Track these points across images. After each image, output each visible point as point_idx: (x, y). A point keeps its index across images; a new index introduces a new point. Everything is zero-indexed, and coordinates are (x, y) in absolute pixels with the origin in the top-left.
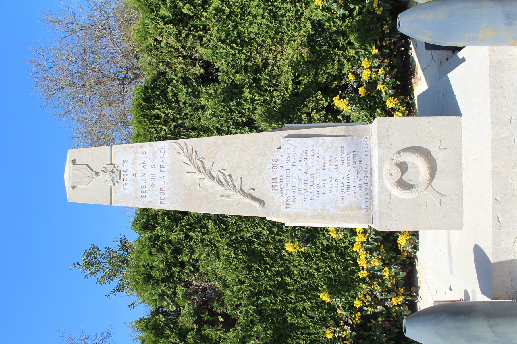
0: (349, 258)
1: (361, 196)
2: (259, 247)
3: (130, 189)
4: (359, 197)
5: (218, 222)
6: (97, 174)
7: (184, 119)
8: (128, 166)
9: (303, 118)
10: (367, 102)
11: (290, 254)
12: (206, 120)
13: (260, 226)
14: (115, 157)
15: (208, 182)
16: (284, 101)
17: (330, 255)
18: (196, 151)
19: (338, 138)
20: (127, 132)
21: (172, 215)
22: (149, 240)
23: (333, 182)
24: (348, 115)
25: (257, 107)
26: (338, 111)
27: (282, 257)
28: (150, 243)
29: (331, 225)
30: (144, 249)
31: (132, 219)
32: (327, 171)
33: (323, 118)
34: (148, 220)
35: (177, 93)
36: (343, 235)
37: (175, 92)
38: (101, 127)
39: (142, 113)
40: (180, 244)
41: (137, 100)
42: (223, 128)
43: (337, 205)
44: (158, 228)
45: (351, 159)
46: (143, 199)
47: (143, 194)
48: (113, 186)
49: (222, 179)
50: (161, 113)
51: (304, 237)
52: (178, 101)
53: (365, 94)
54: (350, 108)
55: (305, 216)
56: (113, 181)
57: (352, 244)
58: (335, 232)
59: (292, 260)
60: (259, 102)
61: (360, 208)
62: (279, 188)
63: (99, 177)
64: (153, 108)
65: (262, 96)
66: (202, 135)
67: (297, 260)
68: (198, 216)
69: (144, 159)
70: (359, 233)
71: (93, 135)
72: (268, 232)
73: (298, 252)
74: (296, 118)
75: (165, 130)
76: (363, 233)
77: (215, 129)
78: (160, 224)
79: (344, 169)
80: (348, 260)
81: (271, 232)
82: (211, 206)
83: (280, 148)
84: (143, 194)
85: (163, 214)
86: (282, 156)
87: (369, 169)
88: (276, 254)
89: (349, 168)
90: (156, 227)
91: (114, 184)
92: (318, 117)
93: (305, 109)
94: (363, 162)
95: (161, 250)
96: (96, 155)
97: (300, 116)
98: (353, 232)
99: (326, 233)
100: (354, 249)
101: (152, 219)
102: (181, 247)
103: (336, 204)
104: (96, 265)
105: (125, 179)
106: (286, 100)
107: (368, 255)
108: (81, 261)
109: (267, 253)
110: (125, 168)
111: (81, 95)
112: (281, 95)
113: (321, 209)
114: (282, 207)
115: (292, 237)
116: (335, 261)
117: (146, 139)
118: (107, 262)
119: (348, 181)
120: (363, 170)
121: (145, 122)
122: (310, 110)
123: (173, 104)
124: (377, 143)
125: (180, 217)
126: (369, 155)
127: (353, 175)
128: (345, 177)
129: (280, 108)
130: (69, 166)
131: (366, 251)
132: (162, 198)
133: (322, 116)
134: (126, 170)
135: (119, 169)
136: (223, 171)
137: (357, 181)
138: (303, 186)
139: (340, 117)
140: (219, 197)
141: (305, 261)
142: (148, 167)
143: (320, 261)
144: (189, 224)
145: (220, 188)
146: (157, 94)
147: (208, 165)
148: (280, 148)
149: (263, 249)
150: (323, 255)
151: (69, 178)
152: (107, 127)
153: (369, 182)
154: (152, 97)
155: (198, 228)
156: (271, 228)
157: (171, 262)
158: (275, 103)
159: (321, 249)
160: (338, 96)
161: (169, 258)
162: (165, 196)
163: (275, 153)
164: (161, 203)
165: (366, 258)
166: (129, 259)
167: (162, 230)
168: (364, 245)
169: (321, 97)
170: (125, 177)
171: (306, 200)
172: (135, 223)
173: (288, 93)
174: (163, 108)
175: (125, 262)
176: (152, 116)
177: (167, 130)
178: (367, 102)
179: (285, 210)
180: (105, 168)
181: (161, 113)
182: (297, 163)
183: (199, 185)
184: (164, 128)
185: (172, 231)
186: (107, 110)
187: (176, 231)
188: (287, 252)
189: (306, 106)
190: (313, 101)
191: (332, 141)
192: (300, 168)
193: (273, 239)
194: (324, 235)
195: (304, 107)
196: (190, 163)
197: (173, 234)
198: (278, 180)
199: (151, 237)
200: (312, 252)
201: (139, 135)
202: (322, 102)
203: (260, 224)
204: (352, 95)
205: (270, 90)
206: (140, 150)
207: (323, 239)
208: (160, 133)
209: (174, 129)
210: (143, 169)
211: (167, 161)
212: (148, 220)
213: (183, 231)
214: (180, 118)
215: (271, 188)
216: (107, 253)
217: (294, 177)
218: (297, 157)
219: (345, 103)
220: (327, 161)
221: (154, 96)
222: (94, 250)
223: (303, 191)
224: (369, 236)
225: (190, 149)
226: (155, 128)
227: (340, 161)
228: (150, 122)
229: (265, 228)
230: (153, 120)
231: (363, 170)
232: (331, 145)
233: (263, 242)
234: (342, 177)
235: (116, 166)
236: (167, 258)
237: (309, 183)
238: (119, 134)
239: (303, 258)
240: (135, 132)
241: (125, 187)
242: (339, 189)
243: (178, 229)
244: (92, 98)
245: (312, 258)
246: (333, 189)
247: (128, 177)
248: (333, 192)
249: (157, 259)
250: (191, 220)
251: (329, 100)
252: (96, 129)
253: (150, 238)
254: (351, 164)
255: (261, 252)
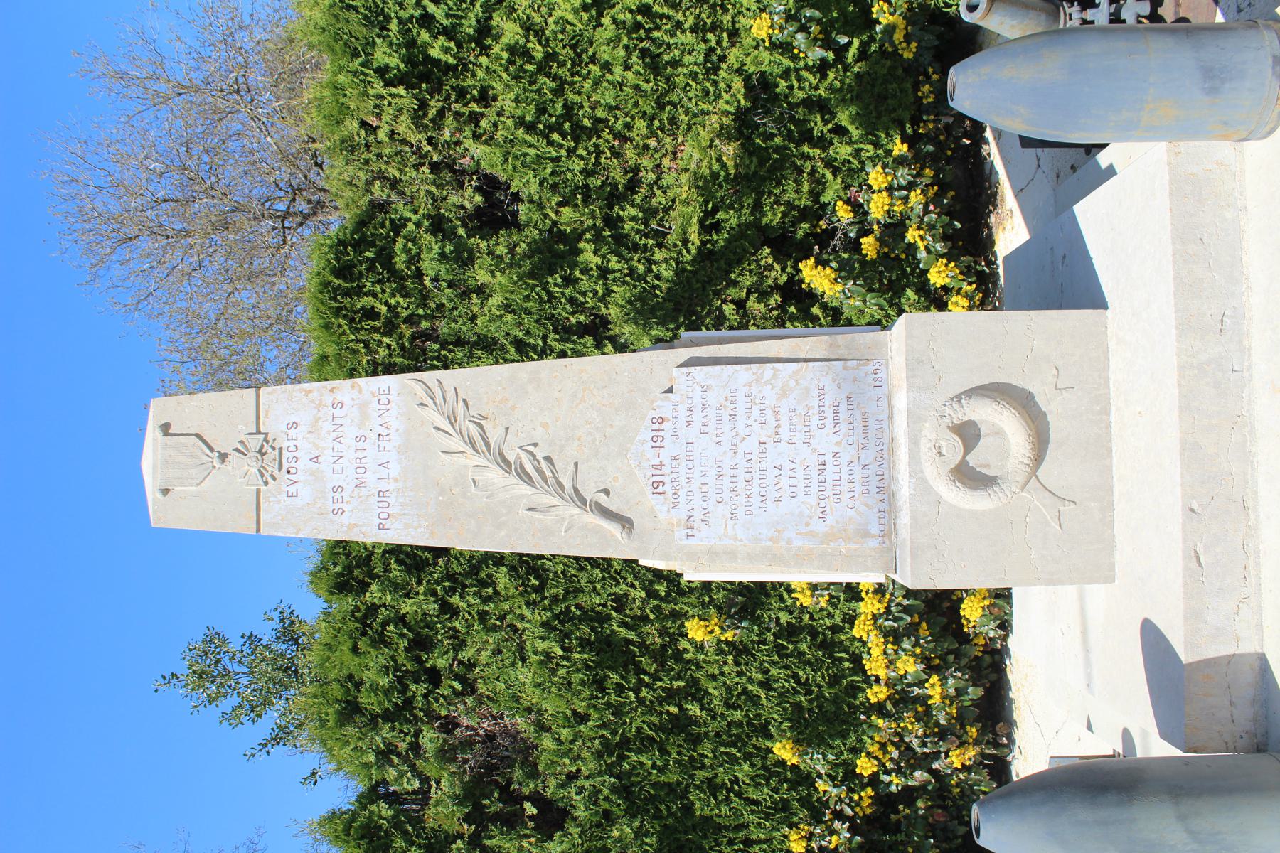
0: (843, 655)
1: (867, 506)
2: (623, 632)
3: (305, 493)
4: (863, 508)
5: (522, 571)
6: (223, 457)
7: (435, 317)
8: (300, 437)
9: (727, 313)
10: (881, 273)
11: (700, 647)
12: (489, 321)
13: (625, 579)
14: (266, 417)
15: (495, 475)
16: (679, 272)
17: (796, 648)
18: (465, 401)
19: (811, 364)
20: (294, 346)
21: (407, 554)
22: (353, 616)
23: (800, 473)
24: (835, 304)
25: (614, 288)
26: (811, 297)
27: (678, 655)
28: (353, 625)
29: (798, 578)
30: (341, 638)
31: (311, 566)
32: (783, 445)
33: (775, 313)
34: (349, 567)
35: (418, 254)
36: (827, 598)
37: (414, 252)
38: (230, 336)
39: (333, 304)
40: (427, 626)
41: (319, 274)
42: (532, 341)
43: (809, 529)
44: (374, 587)
45: (843, 415)
46: (336, 518)
47: (337, 506)
48: (263, 488)
49: (529, 468)
50: (377, 305)
51: (731, 604)
52: (419, 275)
53: (878, 253)
54: (839, 287)
55: (732, 555)
56: (262, 475)
57: (851, 620)
58: (809, 593)
59: (705, 661)
60: (618, 274)
61: (866, 534)
62: (668, 488)
63: (228, 466)
64: (360, 292)
65: (627, 261)
66: (480, 358)
67: (717, 661)
68: (472, 557)
69: (337, 421)
70: (867, 593)
71: (208, 355)
72: (643, 594)
73: (719, 641)
74: (709, 313)
75: (389, 347)
76: (876, 592)
77: (511, 343)
78: (379, 577)
79: (826, 441)
80: (841, 660)
81: (652, 594)
82: (503, 533)
83: (670, 390)
84: (337, 506)
85: (385, 552)
86: (675, 410)
87: (886, 440)
88: (664, 647)
89: (836, 438)
90: (369, 585)
91: (266, 483)
92: (763, 310)
93: (733, 293)
94: (871, 423)
95: (381, 640)
96: (219, 413)
97: (720, 309)
98: (853, 592)
99: (785, 595)
100: (856, 632)
101: (358, 566)
102: (431, 634)
103: (807, 524)
104: (219, 680)
105: (293, 471)
106: (684, 270)
107: (890, 646)
108: (182, 668)
109: (642, 645)
110: (291, 443)
111: (178, 256)
112: (672, 258)
113: (771, 539)
114: (676, 533)
115: (704, 606)
116: (809, 663)
117: (341, 367)
118: (246, 670)
119: (836, 469)
120: (872, 441)
121: (340, 326)
122: (744, 294)
123: (409, 283)
124: (904, 375)
125: (427, 559)
126: (886, 404)
127: (847, 454)
128: (828, 458)
129: (669, 289)
130: (155, 440)
131: (885, 637)
132: (382, 516)
133: (773, 309)
134: (293, 448)
135: (277, 445)
136: (531, 448)
137: (857, 468)
138: (726, 481)
139: (816, 310)
140: (522, 512)
141: (737, 663)
142: (349, 440)
143: (773, 663)
144: (450, 576)
145: (525, 489)
146: (368, 259)
147: (494, 436)
148: (670, 390)
149: (632, 635)
150: (779, 649)
151: (155, 467)
152: (244, 335)
153: (886, 472)
154: (355, 266)
155: (472, 586)
156: (651, 582)
157: (407, 671)
158: (658, 277)
159: (774, 635)
160: (812, 259)
161: (401, 660)
162: (390, 510)
163: (659, 403)
164: (381, 527)
165: (885, 653)
166: (301, 664)
167: (383, 591)
168: (880, 621)
169: (770, 261)
170: (293, 464)
171: (734, 516)
172: (316, 574)
173: (689, 252)
174: (384, 291)
175: (291, 671)
176: (356, 312)
177: (394, 345)
178: (881, 273)
179: (685, 542)
180: (241, 442)
181: (377, 305)
182: (711, 428)
183: (474, 481)
184: (386, 340)
185: (407, 595)
186: (244, 294)
187: (417, 594)
188: (692, 642)
189: (735, 284)
190: (751, 271)
191: (797, 372)
192: (719, 439)
193: (657, 610)
194: (782, 600)
195: (727, 286)
196: (450, 430)
197: (411, 601)
198: (666, 470)
199: (357, 609)
200: (752, 642)
201: (324, 358)
202: (773, 274)
203: (623, 574)
204: (846, 256)
205: (645, 245)
206: (328, 399)
207: (780, 609)
208: (377, 352)
209: (411, 344)
210: (336, 445)
211: (394, 424)
212: (349, 569)
213: (434, 593)
214: (425, 317)
215: (649, 490)
216: (246, 650)
217: (704, 462)
218: (712, 412)
219: (827, 276)
220: (784, 421)
221: (361, 263)
222: (215, 641)
223: (727, 495)
224: (891, 601)
225: (450, 394)
226: (364, 342)
227: (815, 421)
228: (350, 327)
229: (637, 583)
230: (360, 322)
231: (872, 441)
232: (792, 383)
233: (632, 618)
234: (822, 459)
235: (270, 438)
236: (396, 662)
237: (742, 475)
238: (275, 352)
239: (731, 657)
240: (314, 350)
241: (292, 489)
242: (814, 489)
243: (422, 589)
244: (206, 263)
245: (753, 656)
246: (800, 491)
247: (300, 465)
248: (801, 497)
249: (371, 664)
250: (456, 567)
251: (789, 270)
252: (216, 340)
253: (353, 612)
254: (843, 427)
255: (628, 642)
